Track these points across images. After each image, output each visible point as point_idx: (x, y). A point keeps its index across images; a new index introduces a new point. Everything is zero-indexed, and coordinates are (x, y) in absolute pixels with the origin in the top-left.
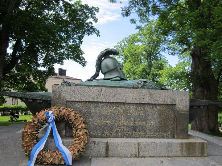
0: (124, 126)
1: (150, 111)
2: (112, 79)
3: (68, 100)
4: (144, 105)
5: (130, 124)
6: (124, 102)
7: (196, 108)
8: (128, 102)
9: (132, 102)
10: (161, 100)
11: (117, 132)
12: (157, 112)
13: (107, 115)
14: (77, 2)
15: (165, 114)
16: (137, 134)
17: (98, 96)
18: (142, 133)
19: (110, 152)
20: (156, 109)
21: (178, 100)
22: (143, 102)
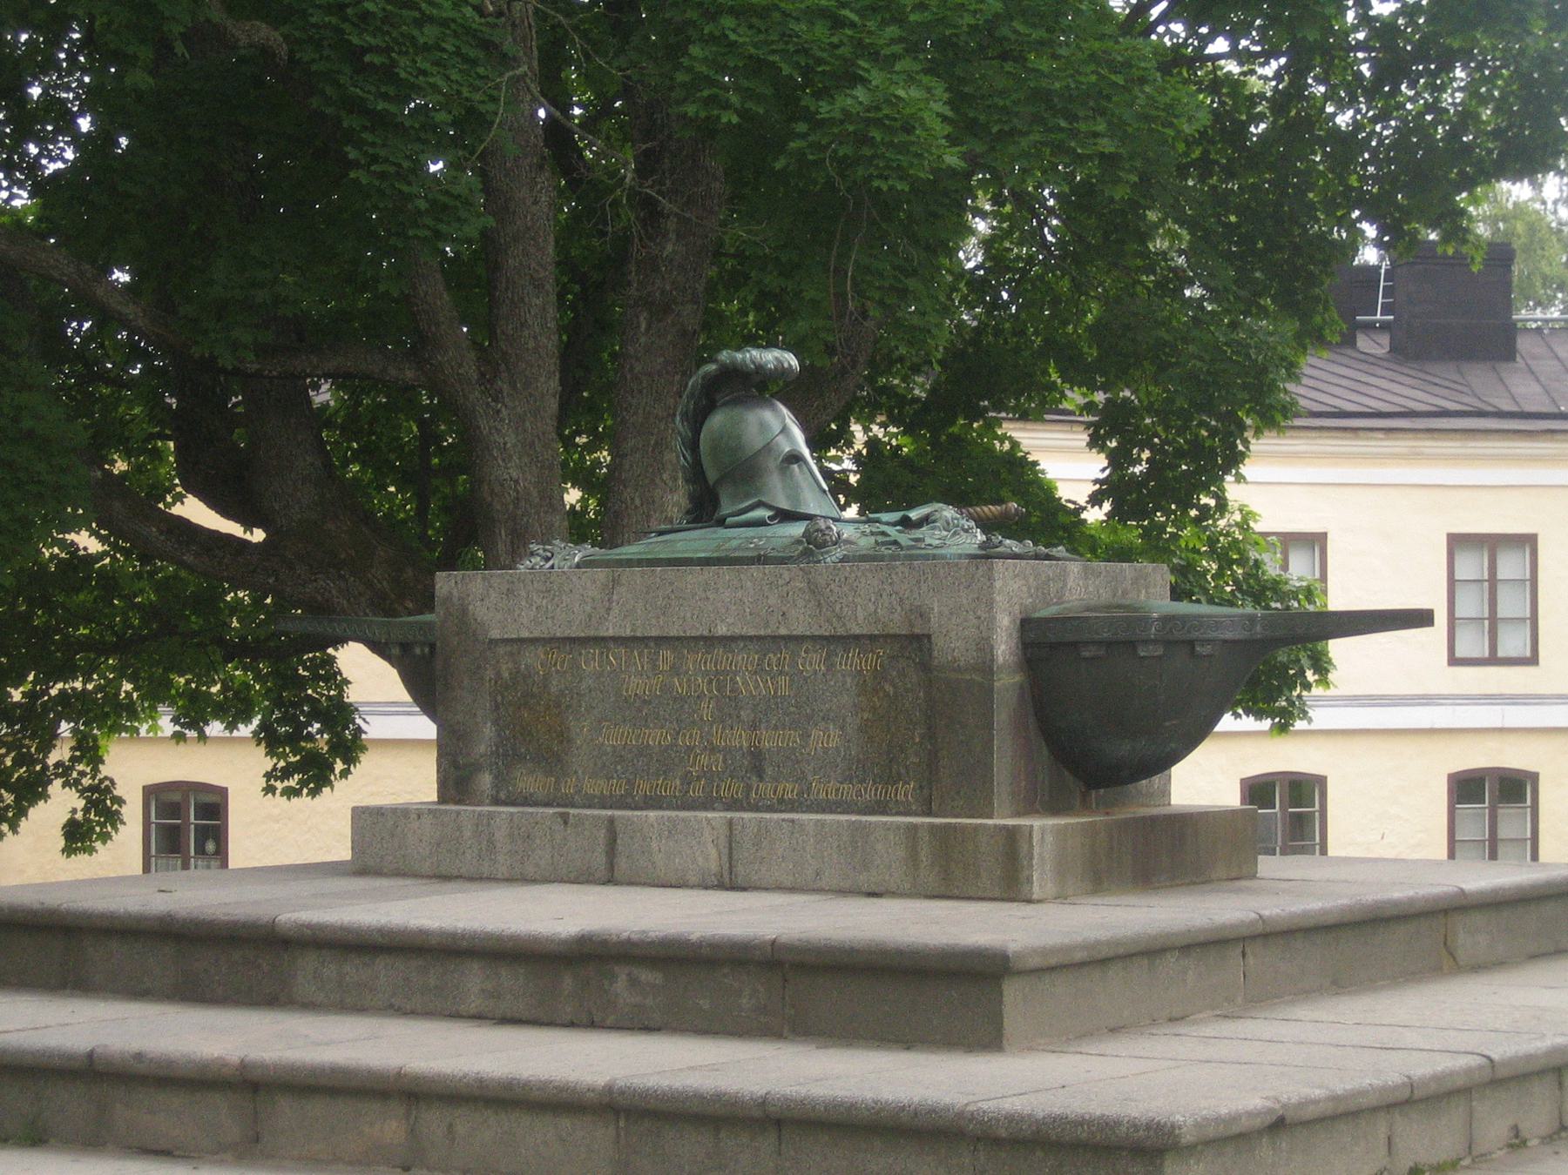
0: (713, 750)
1: (820, 675)
2: (729, 520)
3: (495, 634)
4: (791, 646)
5: (739, 739)
6: (706, 633)
7: (1160, 652)
8: (722, 630)
9: (737, 631)
10: (861, 614)
11: (687, 780)
12: (849, 680)
13: (645, 701)
14: (105, 837)
15: (887, 687)
16: (766, 788)
17: (602, 611)
18: (789, 786)
19: (622, 864)
20: (850, 663)
21: (940, 613)
22: (783, 631)
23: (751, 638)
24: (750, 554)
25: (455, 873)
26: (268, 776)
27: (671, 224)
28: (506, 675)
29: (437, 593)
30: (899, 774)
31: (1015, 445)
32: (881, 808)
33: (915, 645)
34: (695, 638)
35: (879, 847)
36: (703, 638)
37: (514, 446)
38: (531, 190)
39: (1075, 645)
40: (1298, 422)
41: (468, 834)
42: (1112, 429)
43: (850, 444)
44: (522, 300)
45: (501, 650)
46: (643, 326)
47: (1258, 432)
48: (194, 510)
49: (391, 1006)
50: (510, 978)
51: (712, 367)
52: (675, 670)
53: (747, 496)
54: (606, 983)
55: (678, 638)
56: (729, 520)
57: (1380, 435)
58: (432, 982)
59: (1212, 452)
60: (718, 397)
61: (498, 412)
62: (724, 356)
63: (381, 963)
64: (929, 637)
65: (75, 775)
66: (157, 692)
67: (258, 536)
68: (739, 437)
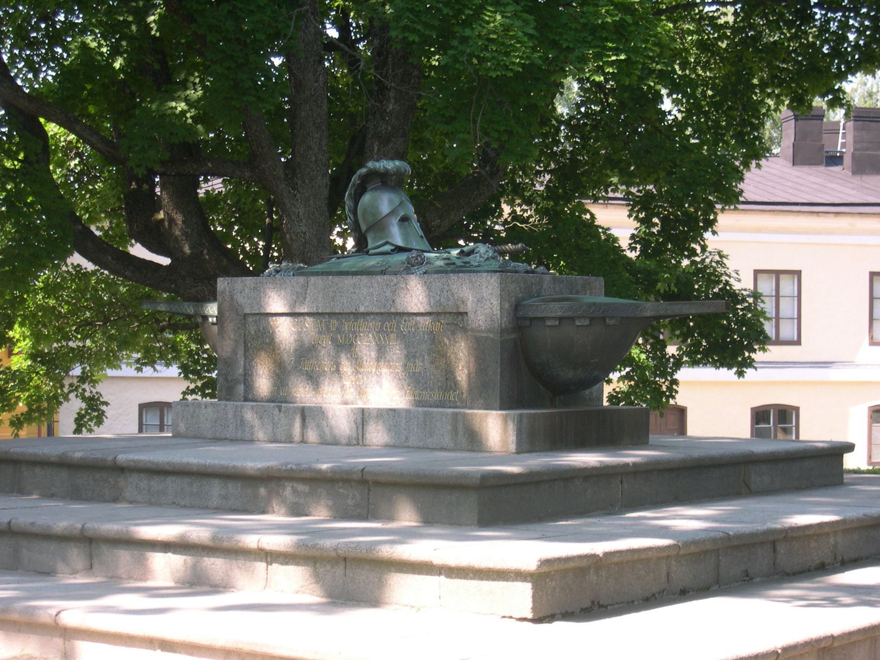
4: (397, 318)
8: (362, 309)
22: (393, 310)
23: (377, 314)
24: (378, 270)
25: (224, 437)
26: (184, 393)
27: (392, 94)
28: (253, 332)
29: (218, 289)
30: (451, 386)
31: (593, 216)
32: (441, 404)
33: (460, 318)
34: (348, 313)
35: (438, 424)
36: (352, 313)
37: (304, 214)
38: (314, 75)
39: (543, 319)
40: (740, 207)
41: (230, 416)
42: (642, 207)
43: (501, 215)
44: (308, 134)
45: (250, 319)
46: (376, 150)
47: (723, 210)
48: (138, 251)
49: (174, 503)
50: (233, 488)
51: (363, 170)
52: (338, 330)
53: (381, 239)
54: (281, 491)
55: (340, 314)
56: (371, 252)
57: (832, 215)
58: (195, 490)
59: (697, 220)
60: (368, 186)
61: (295, 195)
62: (371, 164)
63: (170, 480)
64: (467, 313)
65: (80, 390)
66: (126, 344)
67: (165, 261)
68: (378, 208)
